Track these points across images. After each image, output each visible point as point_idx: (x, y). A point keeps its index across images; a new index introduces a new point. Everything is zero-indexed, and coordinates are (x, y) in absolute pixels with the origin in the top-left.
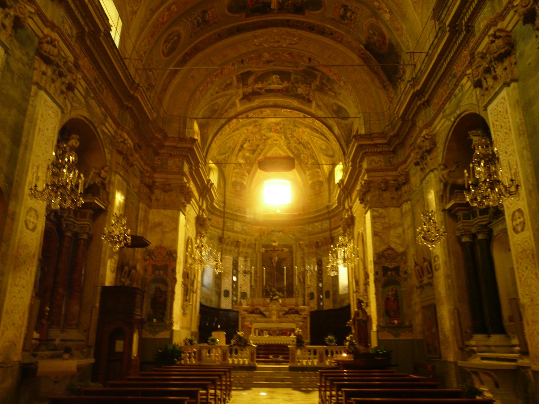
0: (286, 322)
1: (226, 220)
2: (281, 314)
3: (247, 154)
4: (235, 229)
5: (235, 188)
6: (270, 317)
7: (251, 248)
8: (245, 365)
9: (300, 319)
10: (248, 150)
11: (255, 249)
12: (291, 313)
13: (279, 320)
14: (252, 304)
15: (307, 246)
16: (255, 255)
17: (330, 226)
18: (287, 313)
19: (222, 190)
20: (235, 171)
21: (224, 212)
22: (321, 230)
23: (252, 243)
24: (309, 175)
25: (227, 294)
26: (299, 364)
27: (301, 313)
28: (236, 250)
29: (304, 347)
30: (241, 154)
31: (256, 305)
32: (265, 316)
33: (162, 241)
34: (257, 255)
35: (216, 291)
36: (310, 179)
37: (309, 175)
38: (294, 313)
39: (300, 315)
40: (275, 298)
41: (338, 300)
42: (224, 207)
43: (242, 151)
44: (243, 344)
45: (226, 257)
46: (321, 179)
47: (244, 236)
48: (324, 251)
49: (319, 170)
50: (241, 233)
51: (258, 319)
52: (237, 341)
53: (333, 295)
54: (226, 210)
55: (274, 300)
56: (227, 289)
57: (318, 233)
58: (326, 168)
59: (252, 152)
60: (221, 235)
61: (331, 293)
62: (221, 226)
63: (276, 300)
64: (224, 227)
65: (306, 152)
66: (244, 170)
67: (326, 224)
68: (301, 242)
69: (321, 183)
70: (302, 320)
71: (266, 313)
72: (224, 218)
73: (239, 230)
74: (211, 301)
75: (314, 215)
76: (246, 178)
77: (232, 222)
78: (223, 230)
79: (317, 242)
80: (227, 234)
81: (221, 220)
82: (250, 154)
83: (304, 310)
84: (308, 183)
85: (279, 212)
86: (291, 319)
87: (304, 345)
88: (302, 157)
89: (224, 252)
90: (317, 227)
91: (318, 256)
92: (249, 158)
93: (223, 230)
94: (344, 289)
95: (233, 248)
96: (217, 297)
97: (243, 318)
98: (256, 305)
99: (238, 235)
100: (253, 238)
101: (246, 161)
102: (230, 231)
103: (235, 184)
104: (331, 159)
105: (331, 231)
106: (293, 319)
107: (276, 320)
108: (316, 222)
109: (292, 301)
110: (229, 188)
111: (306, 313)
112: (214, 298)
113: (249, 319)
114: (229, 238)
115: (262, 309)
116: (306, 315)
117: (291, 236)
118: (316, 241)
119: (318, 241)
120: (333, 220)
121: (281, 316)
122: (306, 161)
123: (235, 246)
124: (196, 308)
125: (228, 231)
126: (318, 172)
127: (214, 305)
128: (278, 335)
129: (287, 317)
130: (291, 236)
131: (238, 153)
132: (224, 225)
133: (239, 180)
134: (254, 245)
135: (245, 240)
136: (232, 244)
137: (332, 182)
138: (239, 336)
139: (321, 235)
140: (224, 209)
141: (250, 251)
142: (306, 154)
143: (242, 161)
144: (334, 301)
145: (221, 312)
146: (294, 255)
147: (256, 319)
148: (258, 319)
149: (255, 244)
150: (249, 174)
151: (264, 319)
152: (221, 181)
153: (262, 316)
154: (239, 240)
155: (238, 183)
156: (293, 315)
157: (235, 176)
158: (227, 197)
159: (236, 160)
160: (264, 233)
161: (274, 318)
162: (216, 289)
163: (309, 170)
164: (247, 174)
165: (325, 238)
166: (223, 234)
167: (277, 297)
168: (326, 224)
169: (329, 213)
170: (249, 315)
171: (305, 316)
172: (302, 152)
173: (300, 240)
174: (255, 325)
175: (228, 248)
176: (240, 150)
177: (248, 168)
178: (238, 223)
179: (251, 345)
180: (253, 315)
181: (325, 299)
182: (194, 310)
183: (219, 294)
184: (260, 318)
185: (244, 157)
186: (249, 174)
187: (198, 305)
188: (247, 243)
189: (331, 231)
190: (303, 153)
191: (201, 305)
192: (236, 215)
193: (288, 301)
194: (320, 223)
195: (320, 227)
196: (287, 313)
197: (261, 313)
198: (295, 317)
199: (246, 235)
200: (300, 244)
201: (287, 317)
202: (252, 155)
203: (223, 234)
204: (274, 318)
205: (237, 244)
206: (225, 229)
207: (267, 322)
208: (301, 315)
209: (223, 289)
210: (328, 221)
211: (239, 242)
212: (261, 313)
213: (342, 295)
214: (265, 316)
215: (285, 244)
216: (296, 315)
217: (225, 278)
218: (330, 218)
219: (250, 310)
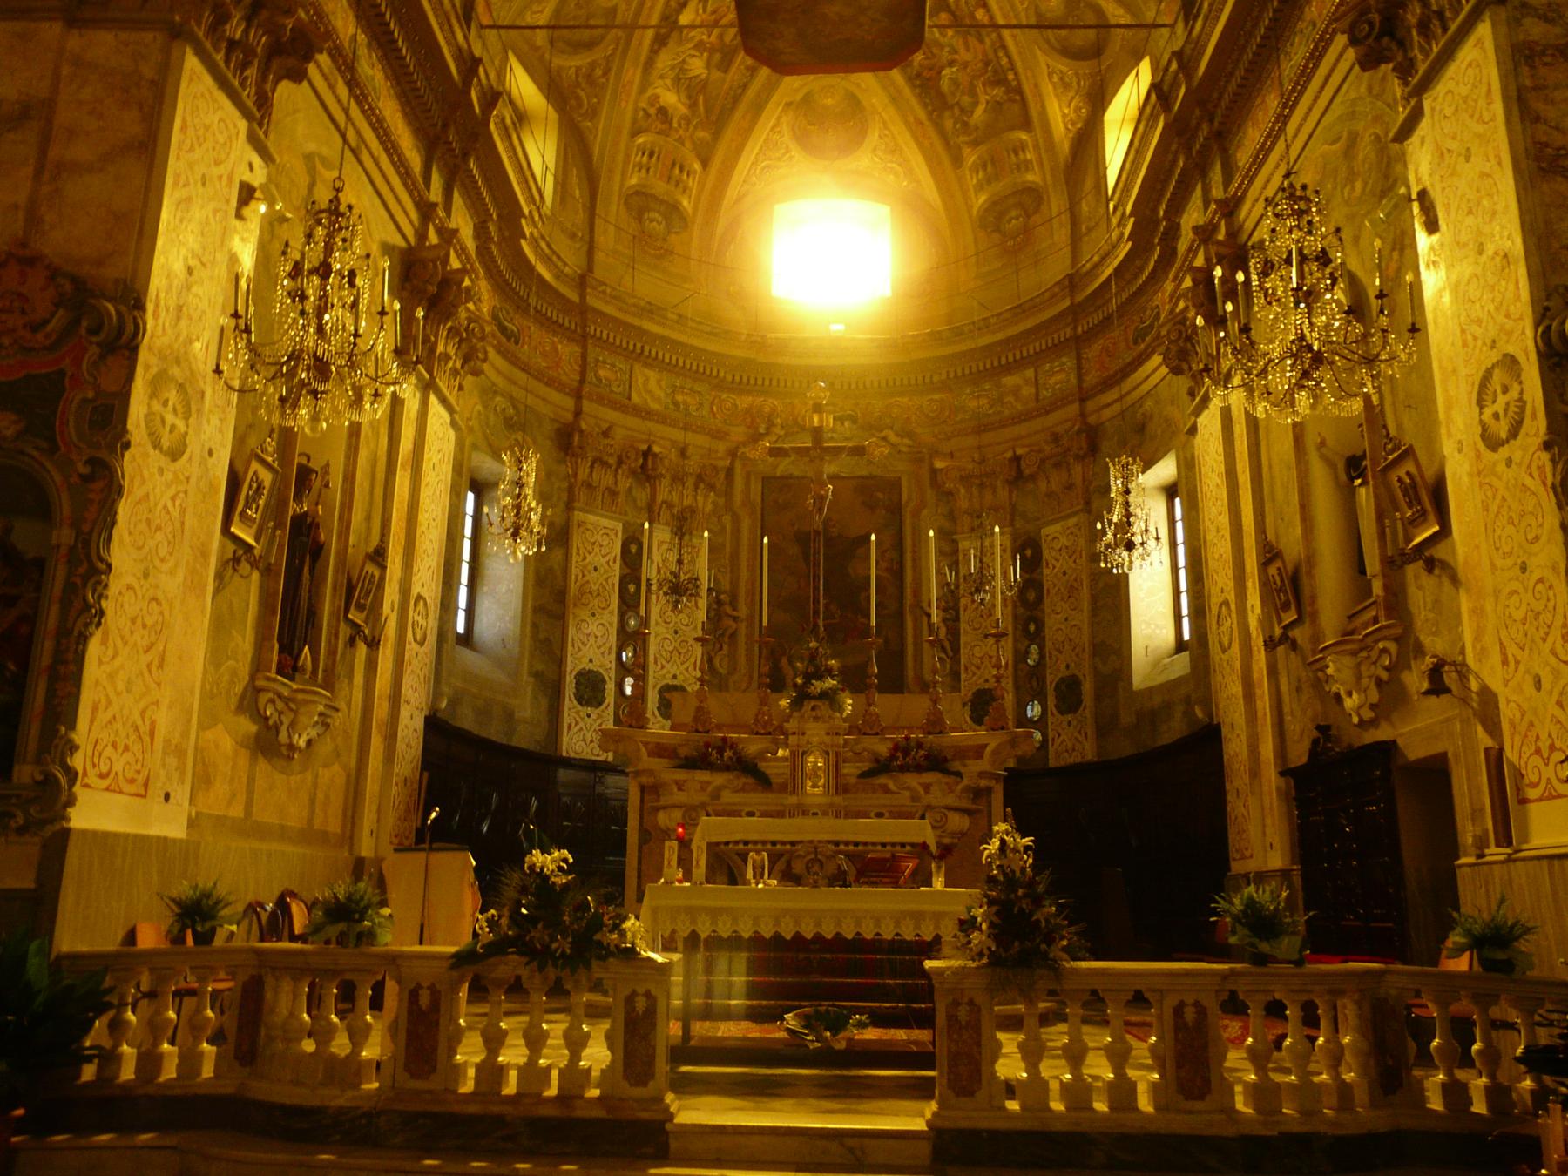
0: (880, 815)
1: (593, 352)
2: (850, 770)
3: (697, 66)
4: (635, 398)
5: (640, 219)
6: (793, 784)
7: (712, 487)
8: (581, 1112)
9: (950, 800)
10: (700, 46)
11: (728, 493)
12: (904, 769)
13: (838, 800)
14: (696, 719)
15: (966, 479)
16: (727, 519)
17: (1080, 377)
18: (882, 767)
19: (581, 217)
20: (641, 140)
21: (583, 311)
22: (1032, 405)
23: (715, 468)
24: (975, 169)
25: (591, 691)
26: (1013, 1106)
27: (956, 766)
28: (642, 496)
29: (1056, 970)
30: (665, 60)
31: (719, 727)
32: (764, 782)
33: (33, 219)
34: (736, 520)
35: (537, 675)
36: (980, 187)
37: (975, 169)
38: (919, 769)
39: (951, 779)
40: (818, 686)
41: (1127, 719)
42: (582, 282)
43: (672, 43)
44: (562, 945)
45: (591, 518)
46: (1031, 177)
47: (677, 435)
48: (1050, 495)
49: (1024, 136)
50: (663, 419)
51: (728, 797)
52: (515, 916)
53: (1098, 698)
54: (593, 301)
55: (810, 697)
56: (591, 667)
57: (1019, 419)
58: (1060, 113)
59: (717, 56)
60: (569, 417)
61: (1087, 687)
62: (569, 374)
63: (828, 696)
64: (582, 381)
65: (964, 56)
66: (681, 140)
67: (1059, 376)
68: (939, 464)
69: (1030, 198)
70: (966, 804)
71: (774, 769)
72: (583, 339)
73: (654, 406)
74: (509, 716)
75: (1000, 336)
76: (692, 183)
77: (621, 364)
78: (578, 395)
79: (1017, 459)
80: (597, 415)
81: (568, 351)
82: (708, 66)
83: (979, 751)
84: (969, 208)
85: (837, 329)
86: (904, 798)
87: (1055, 952)
88: (945, 85)
89: (582, 496)
90: (1016, 392)
91: (1019, 523)
92: (704, 86)
93: (578, 395)
94: (1156, 663)
95: (624, 483)
96: (544, 702)
97: (651, 790)
98: (719, 727)
99: (651, 426)
100: (721, 447)
101: (693, 105)
102: (614, 405)
103: (640, 202)
104: (1085, 67)
105: (1083, 400)
106: (915, 798)
107: (824, 800)
108: (1008, 369)
109: (913, 707)
110: (612, 209)
111: (984, 764)
112: (527, 706)
113: (680, 797)
114: (606, 434)
115: (753, 746)
116: (982, 774)
117: (893, 438)
118: (1009, 454)
119: (1019, 451)
120: (1093, 351)
121: (853, 780)
122: (966, 100)
123: (633, 472)
124: (391, 737)
125: (600, 400)
126: (1020, 148)
127: (524, 738)
128: (839, 879)
129: (886, 790)
130: (893, 438)
131: (654, 51)
132: (583, 373)
133: (660, 187)
134: (722, 475)
135: (683, 453)
136: (620, 462)
137: (1089, 183)
138: (541, 876)
139: (1037, 424)
140: (583, 296)
141: (706, 502)
142: (965, 65)
143: (670, 98)
144: (1105, 728)
145: (563, 775)
146: (908, 520)
147: (716, 796)
148: (728, 797)
149: (730, 472)
150: (705, 164)
151: (758, 799)
152: (574, 179)
153: (750, 780)
154: (656, 449)
155: (654, 197)
156: (912, 780)
157: (640, 166)
158: (599, 256)
159: (643, 88)
160: (770, 425)
161: (814, 791)
162: (540, 667)
163: (975, 143)
164: (697, 166)
165: (1056, 438)
166: (578, 413)
167: (830, 683)
168: (1059, 376)
169: (1075, 312)
170: (681, 775)
171: (983, 783)
172: (945, 55)
173: (935, 453)
174: (709, 830)
175: (604, 479)
176: (660, 41)
177: (701, 134)
178: (653, 375)
179: (631, 953)
180: (702, 776)
181: (1054, 719)
182: (376, 743)
183: (554, 692)
184: (743, 790)
185: (681, 80)
186: (705, 164)
187: (411, 724)
188: (693, 464)
189: (1083, 400)
190: (951, 63)
191: (435, 725)
192: (642, 332)
193: (886, 705)
194: (1030, 373)
195: (1027, 391)
196: (882, 767)
197: (750, 770)
198: (927, 788)
199: (686, 428)
200: (934, 472)
201: (886, 790)
202: (716, 75)
203: (578, 413)
204: (814, 791)
205: (645, 466)
206: (586, 389)
207: (779, 814)
208: (959, 774)
209: (573, 666)
210: (1068, 361)
211: (655, 455)
212: (750, 770)
213: (1150, 691)
214: (764, 782)
215: (865, 473)
216: (929, 777)
217: (584, 614)
218: (1079, 342)
219: (683, 752)
